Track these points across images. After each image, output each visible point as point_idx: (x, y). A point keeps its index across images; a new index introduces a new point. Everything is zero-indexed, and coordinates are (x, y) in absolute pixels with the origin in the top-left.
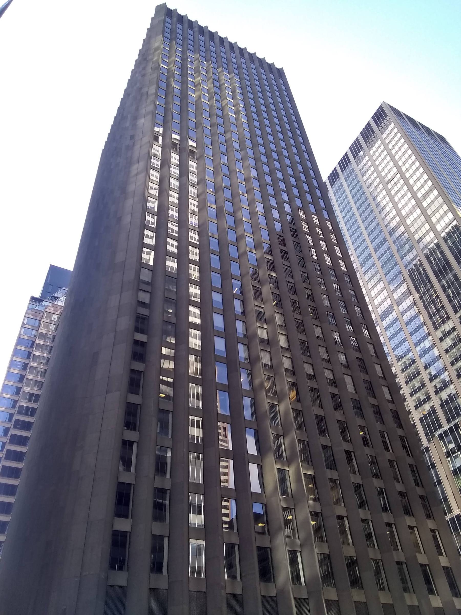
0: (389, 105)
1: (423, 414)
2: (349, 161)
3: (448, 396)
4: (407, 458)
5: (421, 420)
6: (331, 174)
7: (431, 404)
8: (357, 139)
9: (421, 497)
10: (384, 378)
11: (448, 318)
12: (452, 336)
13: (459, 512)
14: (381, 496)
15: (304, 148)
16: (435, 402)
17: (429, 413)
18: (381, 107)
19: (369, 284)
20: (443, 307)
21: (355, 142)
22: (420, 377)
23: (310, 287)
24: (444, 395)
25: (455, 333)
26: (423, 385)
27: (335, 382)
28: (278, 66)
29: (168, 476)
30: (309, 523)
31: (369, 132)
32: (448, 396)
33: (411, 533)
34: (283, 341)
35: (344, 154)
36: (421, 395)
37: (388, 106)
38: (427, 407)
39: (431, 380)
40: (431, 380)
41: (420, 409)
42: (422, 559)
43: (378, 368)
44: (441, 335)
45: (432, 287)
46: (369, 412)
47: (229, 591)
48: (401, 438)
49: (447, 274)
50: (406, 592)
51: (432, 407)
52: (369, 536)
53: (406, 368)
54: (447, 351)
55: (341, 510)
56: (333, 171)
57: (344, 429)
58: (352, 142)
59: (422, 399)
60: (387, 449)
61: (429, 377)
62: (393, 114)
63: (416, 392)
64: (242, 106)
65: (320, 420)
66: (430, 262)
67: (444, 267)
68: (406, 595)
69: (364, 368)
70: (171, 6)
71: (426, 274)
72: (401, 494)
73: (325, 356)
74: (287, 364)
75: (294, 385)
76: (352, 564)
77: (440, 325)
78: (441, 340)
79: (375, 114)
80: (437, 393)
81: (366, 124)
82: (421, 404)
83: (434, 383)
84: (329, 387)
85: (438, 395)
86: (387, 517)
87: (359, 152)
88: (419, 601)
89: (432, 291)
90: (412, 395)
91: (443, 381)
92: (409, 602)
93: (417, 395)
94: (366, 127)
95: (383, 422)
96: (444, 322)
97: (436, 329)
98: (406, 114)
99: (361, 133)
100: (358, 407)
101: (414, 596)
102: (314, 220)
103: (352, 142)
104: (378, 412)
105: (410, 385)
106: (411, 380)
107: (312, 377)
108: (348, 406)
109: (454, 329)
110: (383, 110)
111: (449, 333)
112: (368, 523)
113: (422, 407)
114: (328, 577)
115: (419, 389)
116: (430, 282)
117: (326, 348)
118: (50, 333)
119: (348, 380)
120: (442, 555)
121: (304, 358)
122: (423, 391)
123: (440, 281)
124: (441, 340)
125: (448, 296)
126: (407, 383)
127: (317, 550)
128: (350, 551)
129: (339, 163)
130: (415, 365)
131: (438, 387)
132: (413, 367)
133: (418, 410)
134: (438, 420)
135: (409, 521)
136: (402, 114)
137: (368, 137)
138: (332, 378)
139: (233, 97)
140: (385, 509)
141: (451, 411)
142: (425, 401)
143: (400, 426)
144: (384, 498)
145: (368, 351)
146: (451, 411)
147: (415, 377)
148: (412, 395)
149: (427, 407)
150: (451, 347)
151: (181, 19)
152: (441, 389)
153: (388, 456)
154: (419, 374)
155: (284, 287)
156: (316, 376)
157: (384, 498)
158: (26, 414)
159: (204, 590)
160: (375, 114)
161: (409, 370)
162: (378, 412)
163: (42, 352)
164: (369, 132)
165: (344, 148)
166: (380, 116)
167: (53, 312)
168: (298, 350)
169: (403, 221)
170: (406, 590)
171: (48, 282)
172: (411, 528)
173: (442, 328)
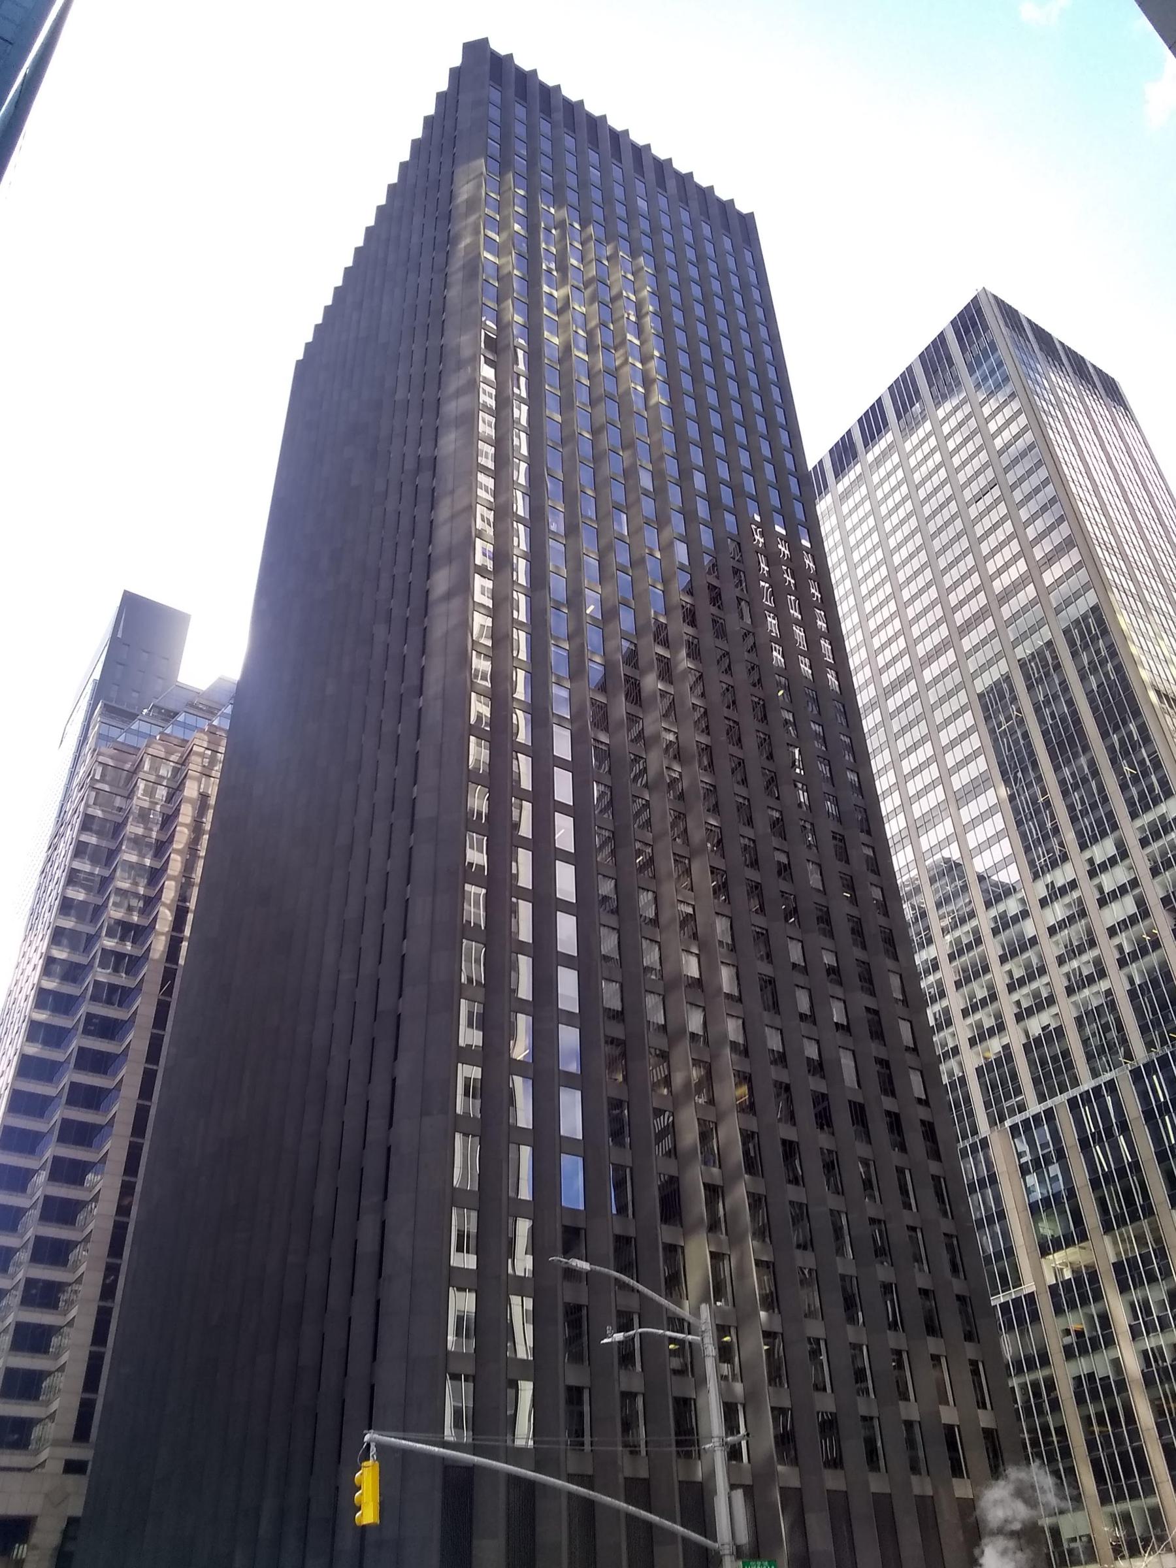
1: (985, 1058)
2: (886, 424)
3: (1043, 1029)
5: (979, 1071)
6: (837, 444)
7: (1005, 1041)
8: (910, 369)
9: (960, 1298)
11: (1065, 858)
12: (1067, 899)
13: (1034, 1289)
14: (889, 1296)
16: (1014, 1037)
17: (998, 1060)
18: (975, 300)
19: (900, 742)
20: (1056, 830)
21: (903, 375)
22: (988, 977)
24: (1035, 1026)
26: (993, 997)
27: (821, 1064)
28: (743, 207)
30: (761, 1348)
33: (934, 1366)
34: (726, 978)
36: (985, 1018)
37: (993, 301)
38: (995, 1046)
39: (1011, 988)
41: (979, 1048)
43: (905, 1029)
44: (1043, 893)
45: (1039, 779)
46: (879, 1127)
47: (628, 1473)
48: (936, 1179)
49: (1076, 756)
50: (914, 1473)
52: (860, 1375)
54: (1052, 931)
55: (816, 1329)
56: (843, 438)
57: (830, 1166)
58: (897, 375)
60: (908, 1206)
61: (1008, 981)
62: (1002, 323)
63: (975, 1008)
64: (656, 353)
65: (790, 1149)
66: (1041, 720)
67: (1070, 738)
68: (914, 1479)
69: (877, 1033)
70: (500, 47)
71: (1029, 745)
72: (924, 1293)
74: (733, 1029)
76: (829, 1425)
78: (1043, 903)
80: (1019, 1018)
82: (982, 1039)
83: (1016, 996)
85: (1022, 1024)
86: (895, 1340)
87: (912, 405)
88: (935, 1488)
90: (965, 1013)
92: (917, 1491)
93: (978, 1016)
94: (934, 342)
95: (903, 1148)
96: (1054, 864)
97: (1036, 876)
99: (921, 356)
100: (859, 1113)
101: (928, 1479)
102: (802, 666)
103: (896, 374)
106: (968, 980)
107: (781, 1059)
108: (842, 1118)
109: (1073, 885)
110: (979, 311)
111: (1063, 891)
113: (984, 1044)
114: (785, 1440)
115: (984, 1003)
116: (1035, 764)
117: (810, 990)
118: (158, 808)
119: (847, 1062)
120: (985, 1407)
121: (767, 1016)
122: (991, 1008)
123: (1057, 768)
124: (1043, 903)
125: (1071, 808)
127: (770, 1398)
128: (826, 1403)
129: (860, 421)
131: (1024, 1005)
132: (975, 953)
133: (975, 1049)
134: (1014, 1076)
135: (934, 1345)
136: (1023, 320)
140: (893, 1326)
141: (1044, 1063)
142: (991, 1032)
143: (935, 1155)
144: (892, 1301)
146: (1044, 1063)
147: (977, 975)
149: (995, 1046)
150: (1062, 925)
151: (525, 82)
152: (1030, 1012)
153: (908, 1218)
154: (986, 969)
157: (892, 1301)
158: (109, 1002)
159: (590, 1472)
160: (961, 315)
162: (895, 1122)
163: (142, 855)
165: (875, 385)
167: (162, 755)
170: (914, 1469)
172: (936, 1358)
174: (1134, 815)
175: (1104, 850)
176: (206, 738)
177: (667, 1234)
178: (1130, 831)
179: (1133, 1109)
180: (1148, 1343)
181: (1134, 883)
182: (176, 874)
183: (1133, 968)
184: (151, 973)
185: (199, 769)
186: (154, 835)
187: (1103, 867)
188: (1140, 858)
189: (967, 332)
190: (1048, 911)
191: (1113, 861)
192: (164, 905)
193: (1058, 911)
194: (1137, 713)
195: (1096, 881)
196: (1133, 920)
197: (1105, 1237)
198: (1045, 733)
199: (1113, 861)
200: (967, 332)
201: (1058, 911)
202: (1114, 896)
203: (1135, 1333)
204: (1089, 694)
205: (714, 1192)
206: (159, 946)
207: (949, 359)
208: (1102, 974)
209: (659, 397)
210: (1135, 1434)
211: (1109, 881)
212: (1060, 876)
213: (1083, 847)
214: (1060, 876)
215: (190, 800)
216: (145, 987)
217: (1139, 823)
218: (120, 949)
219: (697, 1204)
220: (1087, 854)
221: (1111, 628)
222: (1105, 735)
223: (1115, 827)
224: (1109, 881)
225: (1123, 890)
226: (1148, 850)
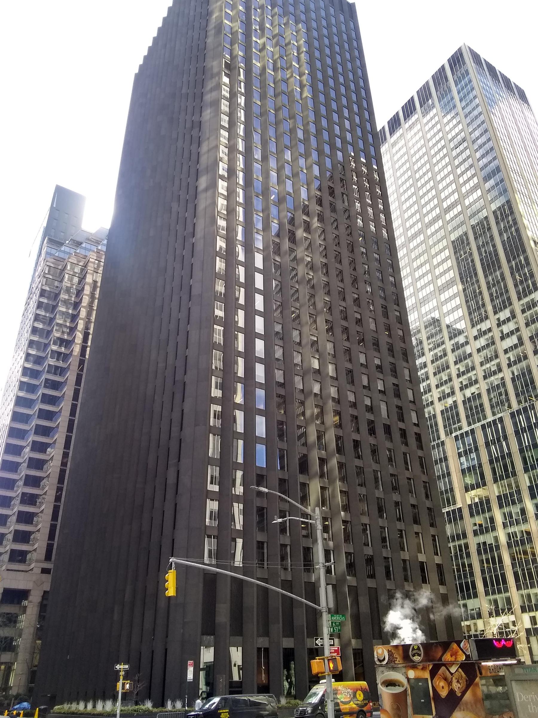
0: (469, 48)
1: (445, 406)
3: (472, 394)
4: (423, 476)
5: (442, 412)
6: (391, 119)
7: (455, 399)
10: (414, 402)
11: (487, 318)
12: (486, 337)
14: (398, 507)
15: (362, 84)
16: (459, 397)
17: (451, 407)
18: (460, 50)
20: (484, 305)
22: (448, 371)
23: (360, 310)
24: (468, 393)
25: (490, 334)
26: (450, 380)
29: (288, 534)
31: (442, 78)
32: (472, 394)
34: (331, 370)
35: (410, 98)
38: (450, 401)
39: (459, 376)
40: (459, 376)
41: (443, 402)
42: (422, 558)
43: (410, 393)
45: (478, 281)
46: (396, 435)
48: (420, 458)
51: (455, 402)
53: (437, 360)
54: (479, 351)
55: (365, 520)
56: (394, 116)
57: (374, 451)
59: (446, 392)
63: (442, 384)
65: (357, 444)
66: (480, 254)
67: (493, 263)
69: (398, 395)
71: (474, 265)
72: (413, 506)
73: (365, 383)
75: (338, 413)
76: (370, 560)
77: (477, 323)
78: (476, 338)
79: (453, 56)
80: (461, 389)
81: (440, 66)
82: (444, 398)
83: (460, 379)
84: (367, 413)
85: (462, 392)
86: (400, 525)
87: (428, 100)
89: (476, 286)
91: (470, 379)
93: (443, 388)
94: (439, 70)
95: (407, 444)
96: (482, 321)
97: (473, 326)
98: (487, 60)
100: (387, 429)
102: (371, 226)
104: (403, 433)
105: (438, 376)
106: (439, 372)
107: (354, 405)
108: (380, 431)
110: (461, 55)
111: (485, 333)
112: (385, 529)
113: (445, 400)
114: (351, 566)
115: (446, 382)
116: (476, 274)
118: (74, 287)
119: (383, 407)
121: (349, 387)
122: (449, 385)
124: (476, 338)
125: (491, 295)
126: (435, 374)
127: (344, 548)
128: (369, 551)
130: (446, 358)
131: (464, 383)
132: (443, 360)
134: (458, 414)
135: (416, 528)
137: (439, 84)
138: (370, 404)
139: (299, 62)
140: (399, 520)
141: (471, 409)
142: (449, 395)
143: (421, 447)
145: (404, 376)
146: (471, 409)
147: (443, 370)
148: (437, 387)
149: (450, 401)
150: (483, 348)
152: (466, 386)
153: (408, 474)
154: (448, 367)
155: (336, 311)
156: (357, 404)
158: (55, 374)
160: (453, 56)
161: (439, 362)
163: (68, 308)
164: (442, 78)
166: (457, 60)
167: (76, 262)
168: (343, 379)
169: (462, 199)
170: (406, 580)
171: (54, 206)
172: (417, 534)
173: (479, 327)
174: (520, 299)
175: (504, 315)
176: (95, 255)
177: (302, 478)
178: (517, 305)
179: (481, 441)
180: (511, 530)
181: (518, 330)
182: (84, 317)
183: (514, 368)
184: (74, 361)
185: (93, 269)
186: (73, 299)
187: (504, 322)
188: (521, 319)
189: (455, 65)
190: (477, 342)
191: (508, 320)
192: (78, 331)
193: (482, 342)
194: (524, 251)
195: (500, 329)
196: (516, 346)
197: (494, 485)
198: (481, 260)
199: (508, 320)
200: (455, 65)
201: (482, 342)
202: (508, 335)
203: (505, 526)
204: (503, 242)
205: (322, 461)
206: (77, 349)
207: (446, 78)
208: (500, 370)
209: (307, 93)
210: (502, 568)
211: (506, 329)
212: (484, 326)
213: (495, 313)
214: (484, 326)
215: (88, 284)
216: (71, 367)
217: (522, 302)
218: (59, 350)
219: (315, 466)
220: (497, 316)
221: (515, 211)
222: (509, 261)
223: (510, 304)
224: (506, 329)
225: (512, 333)
226: (525, 315)
